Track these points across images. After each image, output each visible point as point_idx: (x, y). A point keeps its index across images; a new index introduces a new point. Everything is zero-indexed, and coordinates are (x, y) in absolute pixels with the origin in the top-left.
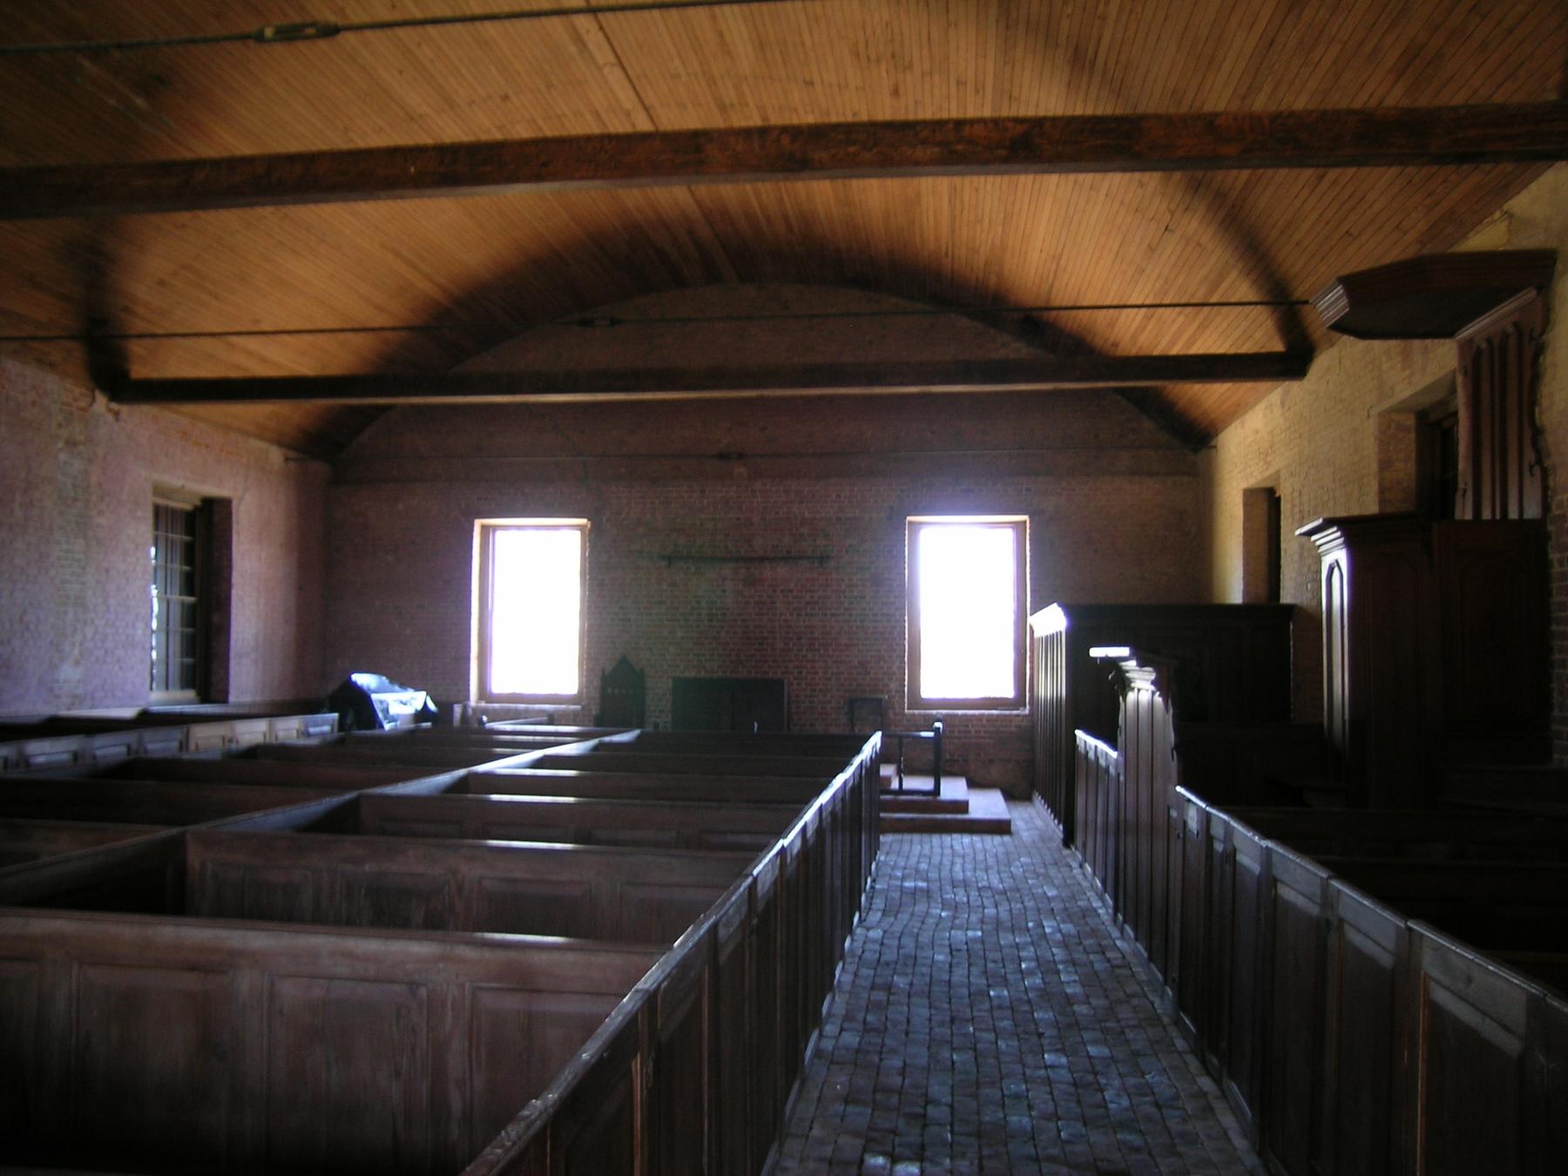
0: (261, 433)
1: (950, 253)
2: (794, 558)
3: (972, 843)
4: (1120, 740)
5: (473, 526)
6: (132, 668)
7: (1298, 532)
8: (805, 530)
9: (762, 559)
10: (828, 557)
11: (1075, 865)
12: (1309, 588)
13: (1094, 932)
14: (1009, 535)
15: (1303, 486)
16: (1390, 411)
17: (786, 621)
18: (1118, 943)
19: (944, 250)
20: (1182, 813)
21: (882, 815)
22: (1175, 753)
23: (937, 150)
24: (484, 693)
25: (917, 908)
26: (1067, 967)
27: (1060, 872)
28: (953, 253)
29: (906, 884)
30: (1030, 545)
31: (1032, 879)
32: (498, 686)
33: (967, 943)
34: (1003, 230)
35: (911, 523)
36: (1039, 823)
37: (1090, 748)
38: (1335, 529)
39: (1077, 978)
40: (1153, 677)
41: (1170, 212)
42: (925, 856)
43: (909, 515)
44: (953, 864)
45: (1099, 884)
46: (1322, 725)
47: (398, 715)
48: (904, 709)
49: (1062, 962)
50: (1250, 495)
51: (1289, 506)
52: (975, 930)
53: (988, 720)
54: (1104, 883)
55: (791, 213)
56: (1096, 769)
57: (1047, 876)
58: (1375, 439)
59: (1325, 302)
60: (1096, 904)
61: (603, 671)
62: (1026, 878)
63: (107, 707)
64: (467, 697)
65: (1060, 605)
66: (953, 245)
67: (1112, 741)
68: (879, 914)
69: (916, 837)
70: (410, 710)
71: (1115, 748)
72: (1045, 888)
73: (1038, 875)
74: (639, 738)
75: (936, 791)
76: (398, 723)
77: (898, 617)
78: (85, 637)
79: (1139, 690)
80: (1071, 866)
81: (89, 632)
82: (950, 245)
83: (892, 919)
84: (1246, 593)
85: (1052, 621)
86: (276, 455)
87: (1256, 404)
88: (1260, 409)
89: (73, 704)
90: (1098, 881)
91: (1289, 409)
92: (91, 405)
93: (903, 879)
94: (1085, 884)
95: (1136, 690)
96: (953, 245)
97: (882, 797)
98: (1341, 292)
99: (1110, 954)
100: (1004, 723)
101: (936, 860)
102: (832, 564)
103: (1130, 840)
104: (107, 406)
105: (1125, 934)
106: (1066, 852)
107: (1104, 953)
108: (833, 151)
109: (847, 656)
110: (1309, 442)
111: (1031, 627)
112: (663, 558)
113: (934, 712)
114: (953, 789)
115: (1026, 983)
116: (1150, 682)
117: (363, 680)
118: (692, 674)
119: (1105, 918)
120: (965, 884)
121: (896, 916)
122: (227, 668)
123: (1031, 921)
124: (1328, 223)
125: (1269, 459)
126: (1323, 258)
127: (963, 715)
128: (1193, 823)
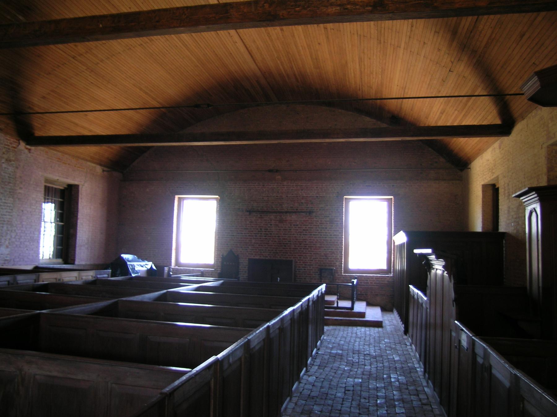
0: (92, 160)
1: (361, 89)
2: (299, 212)
3: (365, 331)
4: (428, 292)
5: (175, 197)
6: (32, 250)
7: (514, 195)
8: (303, 201)
9: (286, 212)
10: (313, 212)
11: (408, 344)
12: (512, 225)
13: (414, 382)
14: (385, 204)
15: (509, 182)
16: (552, 145)
17: (295, 237)
18: (426, 389)
19: (358, 88)
20: (459, 336)
21: (325, 317)
22: (454, 303)
23: (338, 8)
24: (177, 263)
25: (335, 365)
26: (400, 404)
27: (401, 347)
28: (362, 88)
29: (333, 352)
30: (394, 208)
31: (389, 350)
32: (184, 260)
33: (353, 386)
34: (381, 77)
35: (345, 198)
36: (395, 322)
37: (415, 294)
38: (534, 193)
39: (404, 411)
40: (443, 263)
41: (452, 62)
42: (344, 337)
43: (345, 196)
44: (355, 341)
45: (418, 356)
46: (526, 288)
47: (139, 270)
48: (342, 273)
49: (398, 400)
50: (485, 187)
51: (503, 190)
52: (359, 378)
53: (376, 278)
54: (420, 356)
55: (296, 73)
56: (416, 301)
57: (395, 349)
58: (545, 157)
59: (527, 86)
60: (417, 366)
61: (223, 255)
62: (386, 350)
63: (20, 265)
64: (171, 265)
65: (404, 231)
66: (362, 85)
67: (424, 291)
68: (317, 367)
69: (342, 328)
70: (144, 269)
71: (425, 295)
72: (394, 355)
73: (391, 348)
74: (222, 284)
75: (352, 308)
76: (139, 274)
77: (340, 236)
78: (11, 237)
79: (437, 269)
80: (406, 344)
81: (13, 235)
82: (361, 86)
83: (322, 371)
84: (483, 228)
85: (401, 238)
86: (99, 169)
87: (487, 149)
88: (490, 150)
89: (4, 263)
90: (417, 354)
91: (503, 149)
92: (18, 146)
93: (332, 349)
94: (412, 354)
95: (435, 269)
96: (362, 85)
97: (325, 310)
98: (537, 79)
99: (422, 396)
100: (383, 280)
101: (348, 340)
102: (314, 214)
103: (432, 332)
104: (25, 147)
105: (429, 385)
106: (405, 337)
107: (418, 396)
108: (289, 10)
109: (319, 251)
110: (512, 162)
111: (394, 241)
112: (248, 211)
113: (354, 275)
114: (360, 307)
115: (378, 413)
116: (442, 266)
117: (125, 256)
118: (257, 257)
119: (420, 373)
120: (359, 352)
121: (323, 369)
122: (75, 250)
123: (385, 374)
124: (524, 59)
125: (494, 171)
126: (521, 78)
127: (365, 276)
128: (464, 343)
